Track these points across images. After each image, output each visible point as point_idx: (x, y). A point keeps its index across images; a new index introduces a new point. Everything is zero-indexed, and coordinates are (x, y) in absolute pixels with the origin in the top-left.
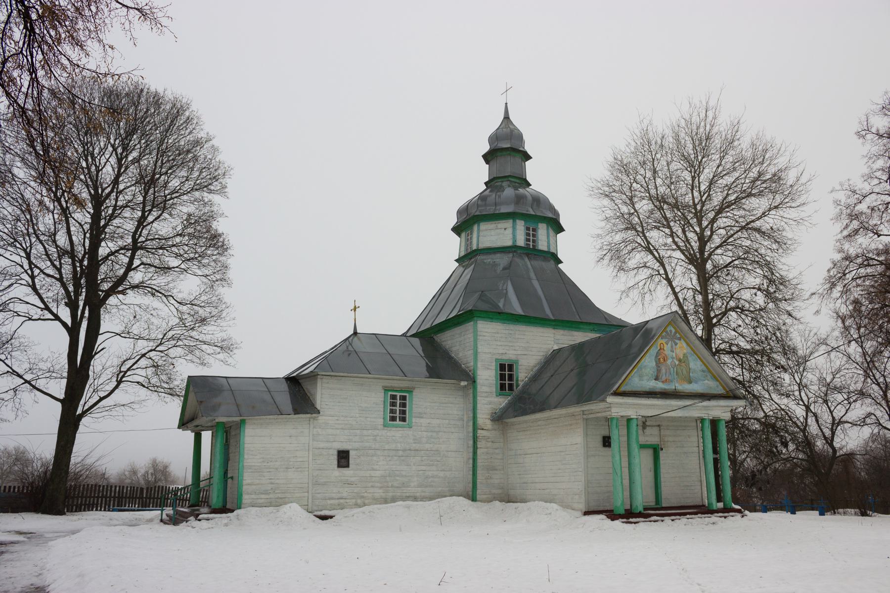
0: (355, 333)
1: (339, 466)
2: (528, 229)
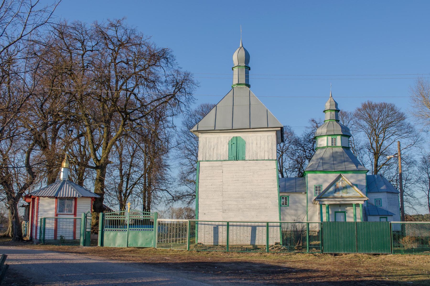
2: (332, 139)
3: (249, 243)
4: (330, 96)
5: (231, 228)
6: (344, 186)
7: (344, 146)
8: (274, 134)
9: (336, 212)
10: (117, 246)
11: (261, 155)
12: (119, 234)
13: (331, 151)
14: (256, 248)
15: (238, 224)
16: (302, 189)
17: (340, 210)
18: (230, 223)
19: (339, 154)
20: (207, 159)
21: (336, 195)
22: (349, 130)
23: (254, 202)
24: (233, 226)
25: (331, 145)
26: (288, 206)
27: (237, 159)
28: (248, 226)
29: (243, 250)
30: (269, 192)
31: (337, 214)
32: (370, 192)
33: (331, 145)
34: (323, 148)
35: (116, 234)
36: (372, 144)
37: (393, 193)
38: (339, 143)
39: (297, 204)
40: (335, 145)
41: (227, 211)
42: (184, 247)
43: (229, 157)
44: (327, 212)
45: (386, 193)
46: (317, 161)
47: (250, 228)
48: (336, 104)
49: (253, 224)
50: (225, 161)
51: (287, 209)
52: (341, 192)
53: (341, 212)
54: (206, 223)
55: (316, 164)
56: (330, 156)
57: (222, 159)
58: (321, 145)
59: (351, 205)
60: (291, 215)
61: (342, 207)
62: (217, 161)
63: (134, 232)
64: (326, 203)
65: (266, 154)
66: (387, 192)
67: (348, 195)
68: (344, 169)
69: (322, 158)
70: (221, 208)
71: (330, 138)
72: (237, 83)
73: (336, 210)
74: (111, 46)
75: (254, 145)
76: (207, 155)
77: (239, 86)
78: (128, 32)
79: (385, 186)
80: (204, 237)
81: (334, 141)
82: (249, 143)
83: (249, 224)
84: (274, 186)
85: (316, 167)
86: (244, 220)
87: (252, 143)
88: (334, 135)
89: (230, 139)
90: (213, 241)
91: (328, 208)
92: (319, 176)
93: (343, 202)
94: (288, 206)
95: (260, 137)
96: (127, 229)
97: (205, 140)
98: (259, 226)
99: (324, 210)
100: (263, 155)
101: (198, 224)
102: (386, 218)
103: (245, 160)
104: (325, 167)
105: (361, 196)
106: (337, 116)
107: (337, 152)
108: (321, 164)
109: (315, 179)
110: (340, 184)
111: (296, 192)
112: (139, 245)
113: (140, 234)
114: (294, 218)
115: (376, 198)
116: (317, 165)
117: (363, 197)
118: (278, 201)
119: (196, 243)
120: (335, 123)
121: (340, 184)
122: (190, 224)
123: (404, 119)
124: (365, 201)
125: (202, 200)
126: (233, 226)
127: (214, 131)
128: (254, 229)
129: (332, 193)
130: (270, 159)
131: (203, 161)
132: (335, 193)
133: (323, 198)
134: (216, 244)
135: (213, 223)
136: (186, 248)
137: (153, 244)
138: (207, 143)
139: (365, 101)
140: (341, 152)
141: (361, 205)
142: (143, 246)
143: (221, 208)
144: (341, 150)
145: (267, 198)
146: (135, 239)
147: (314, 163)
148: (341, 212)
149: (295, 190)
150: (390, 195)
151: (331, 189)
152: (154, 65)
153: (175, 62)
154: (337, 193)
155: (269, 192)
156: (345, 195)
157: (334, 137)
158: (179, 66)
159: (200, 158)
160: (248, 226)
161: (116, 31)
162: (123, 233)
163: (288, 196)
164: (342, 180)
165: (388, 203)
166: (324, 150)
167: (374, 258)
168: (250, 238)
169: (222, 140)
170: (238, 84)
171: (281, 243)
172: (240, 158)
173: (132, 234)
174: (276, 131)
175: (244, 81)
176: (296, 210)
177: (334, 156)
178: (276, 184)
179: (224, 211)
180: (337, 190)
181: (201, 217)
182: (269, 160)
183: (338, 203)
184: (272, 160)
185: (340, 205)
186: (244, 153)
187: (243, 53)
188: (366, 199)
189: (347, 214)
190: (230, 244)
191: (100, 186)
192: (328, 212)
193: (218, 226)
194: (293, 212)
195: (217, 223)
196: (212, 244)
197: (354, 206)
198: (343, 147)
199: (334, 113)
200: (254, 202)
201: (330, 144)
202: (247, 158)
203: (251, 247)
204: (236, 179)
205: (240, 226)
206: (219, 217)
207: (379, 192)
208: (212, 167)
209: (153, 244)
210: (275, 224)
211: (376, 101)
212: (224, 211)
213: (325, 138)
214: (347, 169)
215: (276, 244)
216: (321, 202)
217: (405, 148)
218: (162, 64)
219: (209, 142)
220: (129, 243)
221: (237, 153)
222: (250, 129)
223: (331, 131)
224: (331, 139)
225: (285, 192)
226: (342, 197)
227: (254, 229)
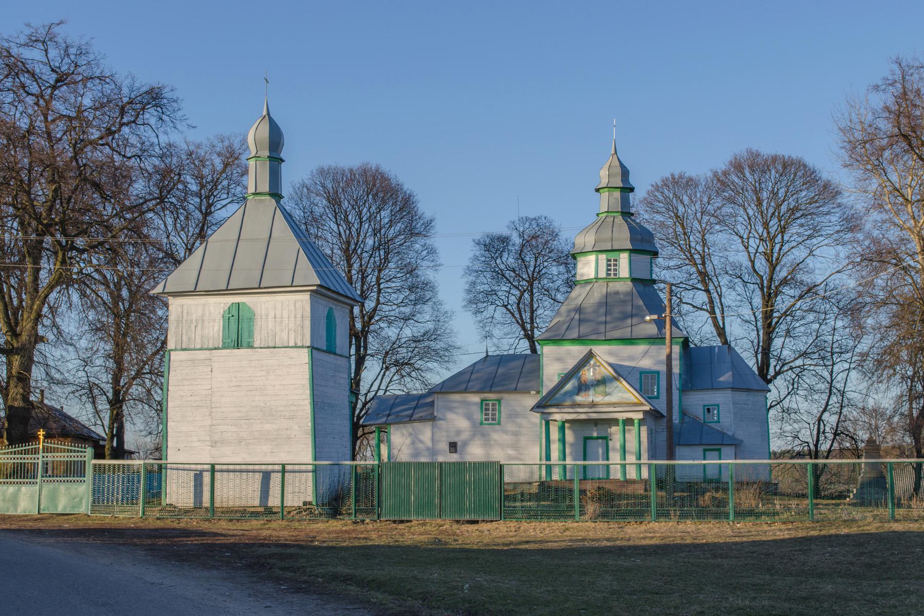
0: (487, 356)
1: (450, 452)
2: (609, 260)
3: (257, 502)
4: (613, 152)
5: (218, 475)
6: (599, 377)
7: (637, 277)
8: (306, 297)
9: (586, 439)
10: (20, 512)
11: (283, 337)
12: (24, 489)
13: (604, 291)
14: (269, 511)
15: (238, 467)
16: (531, 384)
17: (595, 435)
18: (288, 467)
19: (622, 296)
20: (184, 347)
21: (579, 399)
22: (651, 236)
23: (267, 427)
24: (222, 471)
25: (604, 276)
26: (499, 424)
27: (238, 345)
28: (254, 471)
29: (244, 513)
30: (294, 408)
31: (588, 441)
32: (692, 389)
33: (604, 276)
34: (588, 282)
35: (19, 490)
36: (753, 262)
37: (748, 390)
38: (624, 271)
39: (518, 420)
40: (615, 275)
41: (219, 445)
42: (135, 507)
43: (224, 343)
44: (559, 440)
45: (729, 392)
46: (568, 316)
47: (259, 476)
48: (625, 173)
49: (263, 467)
50: (215, 349)
51: (494, 431)
52: (591, 392)
53: (598, 438)
54: (181, 468)
55: (564, 322)
56: (600, 304)
57: (211, 346)
58: (582, 275)
59: (615, 422)
60: (502, 446)
61: (599, 427)
62: (201, 349)
63: (51, 486)
64: (557, 417)
65: (292, 336)
66: (734, 389)
67: (607, 399)
68: (628, 335)
69: (579, 310)
70: (208, 438)
71: (603, 257)
72: (253, 191)
73: (587, 434)
74: (34, 88)
75: (271, 319)
76: (184, 338)
77: (259, 198)
78: (72, 51)
79: (730, 373)
80: (178, 492)
81: (612, 266)
82: (261, 316)
83: (257, 467)
84: (303, 397)
85: (562, 331)
86: (248, 460)
87: (267, 315)
88: (613, 250)
89: (226, 308)
90: (192, 501)
91: (562, 429)
92: (569, 353)
93: (594, 416)
94: (499, 424)
95: (282, 303)
96: (38, 480)
97: (180, 310)
98: (274, 471)
99: (555, 435)
100: (286, 338)
101: (166, 468)
102: (719, 450)
103: (250, 346)
104: (585, 329)
105: (636, 401)
106: (625, 202)
107: (617, 293)
108: (575, 323)
109: (559, 359)
110: (589, 374)
111: (515, 390)
112: (60, 511)
113: (63, 487)
114: (511, 452)
115: (706, 403)
116: (565, 327)
117: (642, 404)
118: (310, 424)
119: (164, 503)
120: (619, 219)
121: (589, 374)
122: (146, 469)
123: (838, 193)
124: (645, 412)
125: (174, 424)
126: (222, 471)
127: (194, 292)
128: (266, 476)
129: (570, 394)
130: (299, 344)
131: (176, 350)
132: (578, 394)
133: (551, 406)
134: (198, 505)
135: (193, 467)
136: (137, 513)
137: (84, 508)
138: (185, 314)
139: (737, 148)
140: (626, 294)
141: (636, 421)
142: (68, 512)
143: (208, 438)
144: (627, 286)
145: (291, 418)
146: (53, 498)
147: (561, 319)
148: (598, 438)
149: (514, 386)
150: (742, 397)
151: (569, 387)
152: (134, 122)
153: (180, 113)
154: (583, 394)
155: (294, 408)
156: (599, 399)
157: (612, 256)
158: (189, 122)
159: (171, 345)
160: (254, 471)
161: (46, 51)
162: (32, 488)
163: (499, 400)
164: (595, 365)
165: (735, 414)
166: (588, 288)
167: (455, 526)
168: (258, 494)
169: (212, 309)
170: (255, 194)
171: (314, 503)
172: (245, 344)
173: (47, 488)
174: (311, 291)
175: (265, 187)
176: (516, 434)
177: (608, 303)
178: (308, 392)
179: (214, 444)
180: (583, 387)
181: (173, 456)
182: (296, 347)
183: (583, 417)
184: (302, 347)
185: (596, 422)
186: (251, 335)
187: (265, 130)
188: (647, 408)
189: (610, 442)
190: (217, 504)
191: (21, 391)
192: (563, 441)
193: (202, 472)
194: (507, 438)
195: (199, 467)
196: (192, 505)
197: (620, 424)
198: (634, 280)
199: (617, 194)
200: (267, 427)
201: (602, 274)
202: (256, 344)
203: (262, 509)
204: (235, 384)
205: (241, 471)
206: (204, 456)
207: (712, 389)
208: (193, 361)
209: (84, 508)
210: (303, 467)
211: (767, 150)
212: (214, 444)
213: (592, 257)
214: (634, 336)
215: (305, 503)
216: (545, 416)
217: (838, 272)
218: (153, 121)
219: (188, 313)
220: (42, 507)
221: (238, 334)
222: (259, 288)
223: (605, 241)
224: (605, 261)
225: (490, 392)
226: (593, 405)
227: (266, 476)
